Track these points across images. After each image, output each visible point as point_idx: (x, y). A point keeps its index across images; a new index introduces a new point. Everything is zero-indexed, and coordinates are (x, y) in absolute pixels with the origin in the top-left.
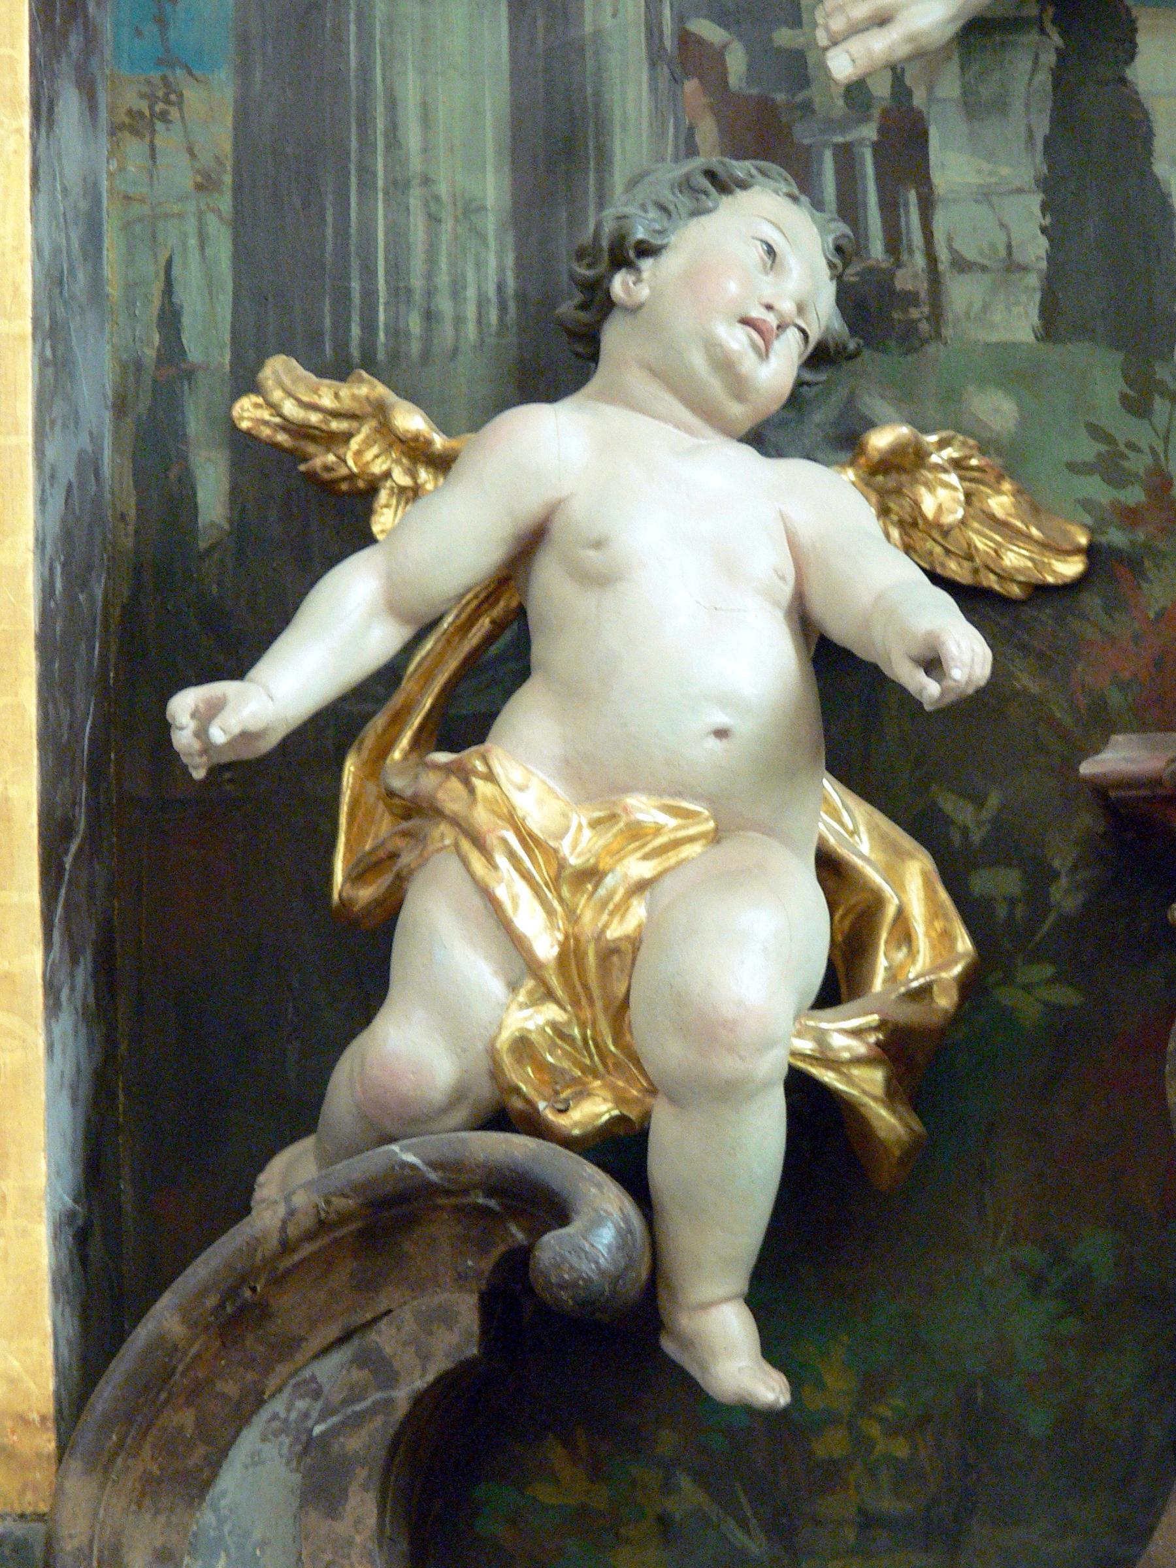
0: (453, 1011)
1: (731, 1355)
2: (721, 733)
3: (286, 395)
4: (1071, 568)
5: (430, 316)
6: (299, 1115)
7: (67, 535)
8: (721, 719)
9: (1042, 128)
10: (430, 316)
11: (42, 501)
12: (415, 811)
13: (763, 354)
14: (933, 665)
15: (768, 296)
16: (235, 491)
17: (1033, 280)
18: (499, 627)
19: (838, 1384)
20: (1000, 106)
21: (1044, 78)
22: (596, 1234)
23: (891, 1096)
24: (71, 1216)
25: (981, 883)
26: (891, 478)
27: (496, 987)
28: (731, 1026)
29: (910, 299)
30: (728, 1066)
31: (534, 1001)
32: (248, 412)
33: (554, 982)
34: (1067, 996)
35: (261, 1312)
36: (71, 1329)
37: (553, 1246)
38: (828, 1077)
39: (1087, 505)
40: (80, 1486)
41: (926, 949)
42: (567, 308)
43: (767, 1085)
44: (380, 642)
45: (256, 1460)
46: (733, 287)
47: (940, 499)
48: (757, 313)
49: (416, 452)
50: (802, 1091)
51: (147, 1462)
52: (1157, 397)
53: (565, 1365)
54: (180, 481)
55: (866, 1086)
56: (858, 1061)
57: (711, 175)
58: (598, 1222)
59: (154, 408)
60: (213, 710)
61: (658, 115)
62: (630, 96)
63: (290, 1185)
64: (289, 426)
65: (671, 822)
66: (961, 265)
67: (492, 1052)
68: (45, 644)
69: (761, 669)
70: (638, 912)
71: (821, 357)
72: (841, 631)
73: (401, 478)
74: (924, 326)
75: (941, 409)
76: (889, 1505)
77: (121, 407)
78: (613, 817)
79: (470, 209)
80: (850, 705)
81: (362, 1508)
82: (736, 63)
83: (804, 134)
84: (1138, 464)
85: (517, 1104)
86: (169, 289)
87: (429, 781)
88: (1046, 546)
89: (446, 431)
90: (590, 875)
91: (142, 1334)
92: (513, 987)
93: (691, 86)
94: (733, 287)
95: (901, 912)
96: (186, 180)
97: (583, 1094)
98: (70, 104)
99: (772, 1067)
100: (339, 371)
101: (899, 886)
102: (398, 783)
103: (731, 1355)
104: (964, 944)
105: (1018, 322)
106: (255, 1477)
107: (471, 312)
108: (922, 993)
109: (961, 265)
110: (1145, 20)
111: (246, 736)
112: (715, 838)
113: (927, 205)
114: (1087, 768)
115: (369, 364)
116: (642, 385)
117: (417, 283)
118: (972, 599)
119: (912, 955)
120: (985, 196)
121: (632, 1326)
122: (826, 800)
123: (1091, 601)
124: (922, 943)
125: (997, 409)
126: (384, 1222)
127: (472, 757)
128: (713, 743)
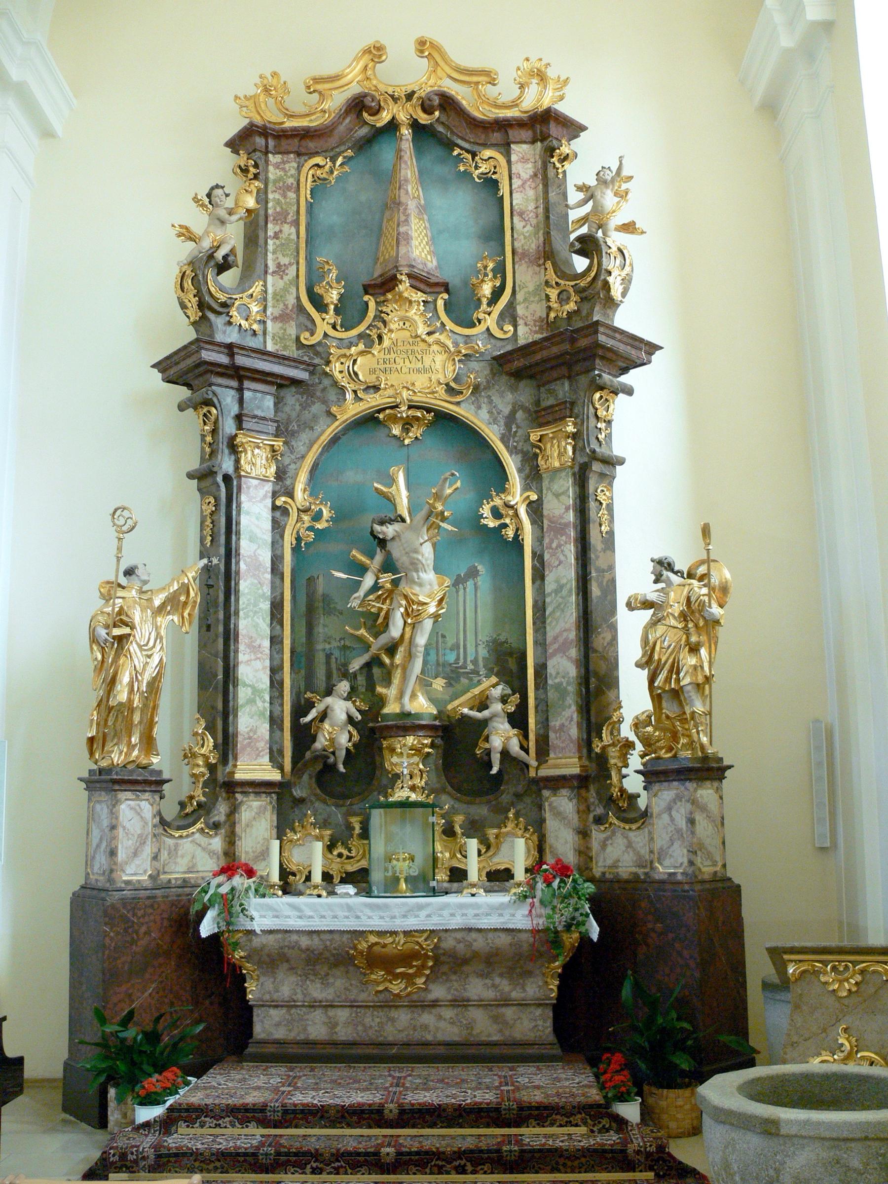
0: (321, 742)
1: (341, 768)
3: (308, 695)
6: (309, 748)
26: (354, 702)
41: (356, 738)
44: (316, 715)
47: (358, 704)
52: (386, 710)
53: (329, 769)
54: (274, 894)
63: (308, 755)
69: (344, 717)
71: (349, 693)
80: (350, 719)
81: (314, 780)
103: (341, 768)
105: (364, 690)
106: (305, 777)
121: (335, 765)
125: (362, 696)
126: (316, 758)
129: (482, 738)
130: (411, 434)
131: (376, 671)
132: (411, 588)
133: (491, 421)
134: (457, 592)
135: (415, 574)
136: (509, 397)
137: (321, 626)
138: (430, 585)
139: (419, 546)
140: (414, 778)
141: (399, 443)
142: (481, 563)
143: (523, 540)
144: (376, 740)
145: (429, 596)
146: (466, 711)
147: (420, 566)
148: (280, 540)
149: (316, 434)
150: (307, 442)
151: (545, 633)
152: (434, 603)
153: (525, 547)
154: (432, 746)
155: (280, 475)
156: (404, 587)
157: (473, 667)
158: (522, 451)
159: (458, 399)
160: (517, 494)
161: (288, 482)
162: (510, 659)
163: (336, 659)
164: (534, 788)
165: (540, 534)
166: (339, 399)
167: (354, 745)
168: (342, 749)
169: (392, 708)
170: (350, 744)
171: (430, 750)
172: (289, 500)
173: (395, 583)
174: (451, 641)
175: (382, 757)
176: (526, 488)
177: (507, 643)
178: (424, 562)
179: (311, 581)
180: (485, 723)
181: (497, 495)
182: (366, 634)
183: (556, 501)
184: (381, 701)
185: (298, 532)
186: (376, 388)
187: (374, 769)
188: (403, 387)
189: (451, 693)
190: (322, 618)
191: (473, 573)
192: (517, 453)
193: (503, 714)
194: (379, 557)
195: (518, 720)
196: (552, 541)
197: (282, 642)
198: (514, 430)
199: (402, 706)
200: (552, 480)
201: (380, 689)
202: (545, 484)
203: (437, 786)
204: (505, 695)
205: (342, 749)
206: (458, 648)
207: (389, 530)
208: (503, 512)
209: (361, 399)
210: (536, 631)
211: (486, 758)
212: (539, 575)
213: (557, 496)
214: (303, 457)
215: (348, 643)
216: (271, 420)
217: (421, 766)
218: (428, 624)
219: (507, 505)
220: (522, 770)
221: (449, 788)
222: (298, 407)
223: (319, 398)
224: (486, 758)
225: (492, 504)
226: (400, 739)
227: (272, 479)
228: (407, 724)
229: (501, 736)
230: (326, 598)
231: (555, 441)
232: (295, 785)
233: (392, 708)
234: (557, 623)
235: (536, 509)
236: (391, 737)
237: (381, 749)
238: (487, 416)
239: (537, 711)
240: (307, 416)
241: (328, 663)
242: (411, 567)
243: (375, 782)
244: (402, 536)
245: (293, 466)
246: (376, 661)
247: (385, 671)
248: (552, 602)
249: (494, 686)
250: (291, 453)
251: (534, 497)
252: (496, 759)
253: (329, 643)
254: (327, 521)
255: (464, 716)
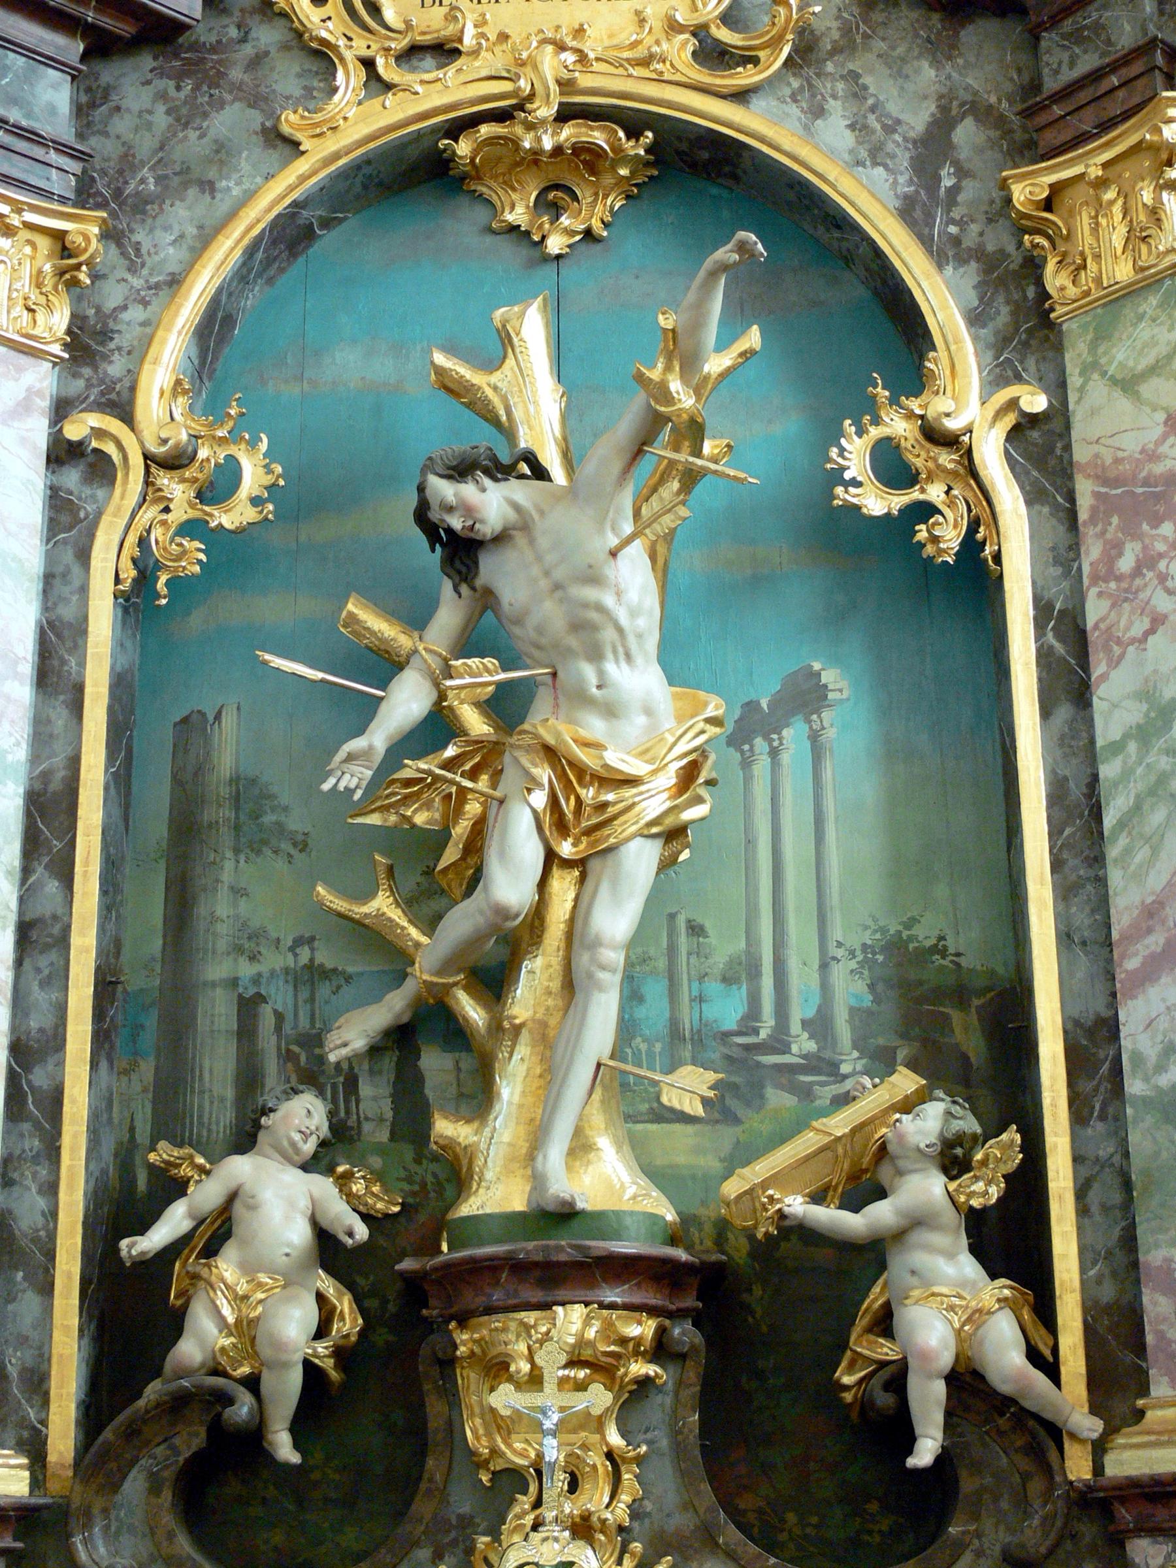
0: (203, 1338)
1: (284, 1448)
2: (287, 1255)
3: (164, 1152)
4: (397, 1209)
5: (209, 1130)
7: (95, 1192)
8: (287, 1250)
9: (392, 1080)
10: (209, 1130)
11: (87, 1182)
12: (195, 1277)
13: (305, 1142)
14: (350, 1234)
15: (307, 1124)
16: (149, 1181)
17: (388, 1123)
18: (224, 1222)
19: (318, 1457)
20: (380, 1072)
21: (393, 1064)
22: (243, 1408)
23: (336, 1367)
24: (84, 1401)
25: (367, 1303)
26: (343, 1181)
27: (215, 1331)
28: (286, 1344)
29: (352, 1128)
30: (284, 1357)
31: (227, 1336)
32: (152, 1157)
33: (233, 1330)
34: (391, 1338)
35: (139, 1432)
36: (81, 1437)
37: (228, 1412)
38: (316, 1361)
39: (402, 1190)
40: (78, 1488)
41: (349, 1322)
42: (248, 1128)
43: (297, 1363)
44: (186, 1225)
45: (135, 1479)
46: (297, 1121)
47: (358, 1187)
48: (304, 1129)
49: (202, 1170)
50: (308, 1365)
51: (101, 1479)
52: (468, 1208)
55: (328, 1364)
56: (325, 1356)
57: (292, 1089)
58: (243, 1404)
59: (126, 1155)
60: (133, 1244)
61: (279, 1072)
62: (271, 1066)
63: (153, 1391)
64: (164, 1161)
65: (271, 1281)
66: (367, 1119)
67: (213, 1351)
68: (85, 1224)
69: (299, 1234)
70: (260, 1309)
71: (323, 1144)
72: (325, 1224)
73: (196, 1177)
74: (356, 1137)
75: (361, 1162)
76: (333, 1495)
77: (116, 1155)
78: (253, 1280)
79: (222, 1100)
80: (327, 1247)
81: (167, 1495)
82: (303, 1058)
83: (322, 1080)
84: (417, 1179)
85: (221, 1368)
86: (132, 1120)
87: (198, 1269)
88: (388, 1202)
89: (211, 1163)
90: (246, 1297)
91: (101, 1439)
92: (221, 1331)
93: (289, 1065)
94: (297, 1121)
95: (341, 1311)
96: (139, 1089)
97: (242, 1365)
98: (104, 1064)
99: (298, 1357)
100: (180, 1145)
101: (342, 1304)
102: (190, 1269)
103: (284, 1448)
104: (360, 1321)
105: (383, 1136)
106: (134, 1485)
107: (222, 1130)
108: (347, 1336)
109: (367, 1119)
110: (423, 1048)
111: (143, 1253)
112: (284, 1287)
113: (358, 1101)
114: (397, 1267)
115: (191, 1145)
116: (269, 1150)
117: (206, 1120)
118: (366, 1218)
119: (344, 1325)
120: (375, 1099)
122: (320, 1276)
123: (402, 1220)
124: (348, 1321)
125: (376, 1162)
126: (179, 1404)
127: (212, 1261)
128: (284, 1258)
129: (861, 1323)
130: (565, 221)
131: (434, 1063)
132: (572, 721)
133: (863, 154)
134: (746, 764)
135: (589, 672)
136: (927, 74)
137: (223, 893)
138: (648, 711)
139: (603, 555)
140: (586, 1486)
141: (525, 252)
142: (835, 660)
143: (997, 558)
144: (428, 1323)
145: (643, 754)
146: (796, 1205)
147: (608, 635)
148: (76, 570)
149: (223, 206)
150: (191, 230)
151: (1102, 904)
152: (669, 778)
153: (1008, 584)
154: (660, 1350)
155: (85, 344)
156: (546, 722)
157: (811, 1046)
158: (979, 254)
159: (745, 77)
160: (968, 395)
161: (115, 368)
162: (956, 1016)
163: (279, 1017)
164: (1088, 1531)
165: (1057, 531)
166: (308, 90)
167: (340, 1354)
168: (286, 1365)
169: (496, 1195)
170: (322, 1348)
171: (651, 1369)
172: (114, 425)
173: (506, 706)
174: (724, 947)
175: (452, 1397)
176: (1001, 374)
177: (943, 953)
178: (624, 620)
179: (192, 729)
180: (872, 1254)
181: (894, 401)
182: (396, 915)
183: (1123, 403)
184: (456, 1174)
185: (143, 542)
186: (445, 51)
187: (421, 1452)
188: (545, 41)
189: (727, 1146)
190: (229, 865)
191: (805, 696)
192: (961, 261)
193: (950, 1216)
194: (449, 616)
195: (1009, 1239)
196: (1114, 550)
197: (63, 942)
198: (947, 182)
199: (538, 1181)
200: (1102, 335)
201: (445, 1127)
202: (1075, 356)
203: (681, 1522)
204: (959, 1140)
205: (286, 1365)
206: (754, 973)
207: (490, 503)
208: (919, 463)
209: (388, 87)
210: (1064, 893)
211: (885, 1400)
212: (1070, 682)
213: (1128, 384)
214: (175, 282)
215: (325, 957)
216: (62, 148)
217: (614, 1438)
218: (640, 860)
219: (934, 435)
220: (1036, 1453)
221: (731, 1535)
222: (161, 119)
223: (238, 88)
224: (885, 1400)
225: (875, 432)
226: (530, 1317)
227: (56, 349)
228: (556, 1256)
229: (946, 1308)
230: (247, 794)
231: (1110, 195)
232: (87, 1525)
233: (496, 1195)
234: (1155, 851)
235: (1041, 444)
236: (490, 1311)
237: (447, 1363)
238: (848, 139)
239: (1083, 1210)
240: (192, 146)
241: (246, 1032)
242: (573, 641)
243: (422, 1507)
244: (539, 525)
245: (135, 314)
246: (431, 1022)
247: (467, 1062)
248: (1127, 774)
249: (907, 1106)
250: (132, 269)
251: (1036, 402)
252: (928, 1402)
253: (253, 958)
254: (256, 501)
255: (793, 1231)
